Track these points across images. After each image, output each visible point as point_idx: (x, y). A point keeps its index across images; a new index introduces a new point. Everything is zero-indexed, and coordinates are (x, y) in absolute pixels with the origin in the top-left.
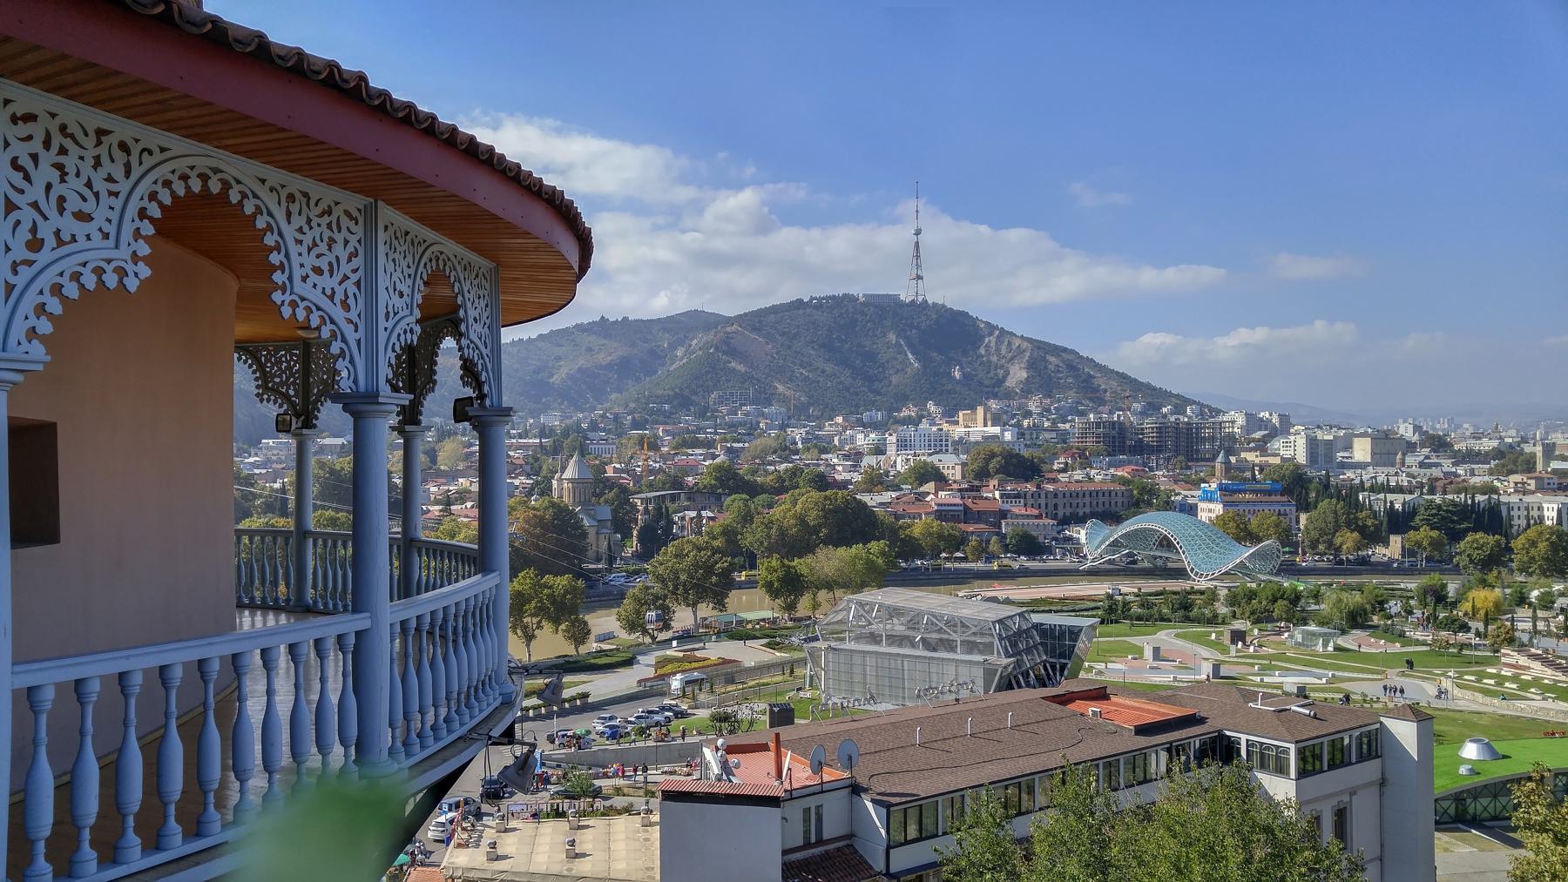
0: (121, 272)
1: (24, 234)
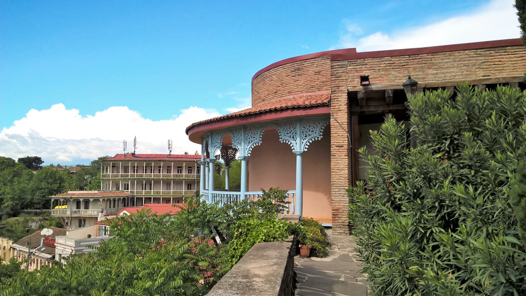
0: (318, 138)
1: (305, 135)
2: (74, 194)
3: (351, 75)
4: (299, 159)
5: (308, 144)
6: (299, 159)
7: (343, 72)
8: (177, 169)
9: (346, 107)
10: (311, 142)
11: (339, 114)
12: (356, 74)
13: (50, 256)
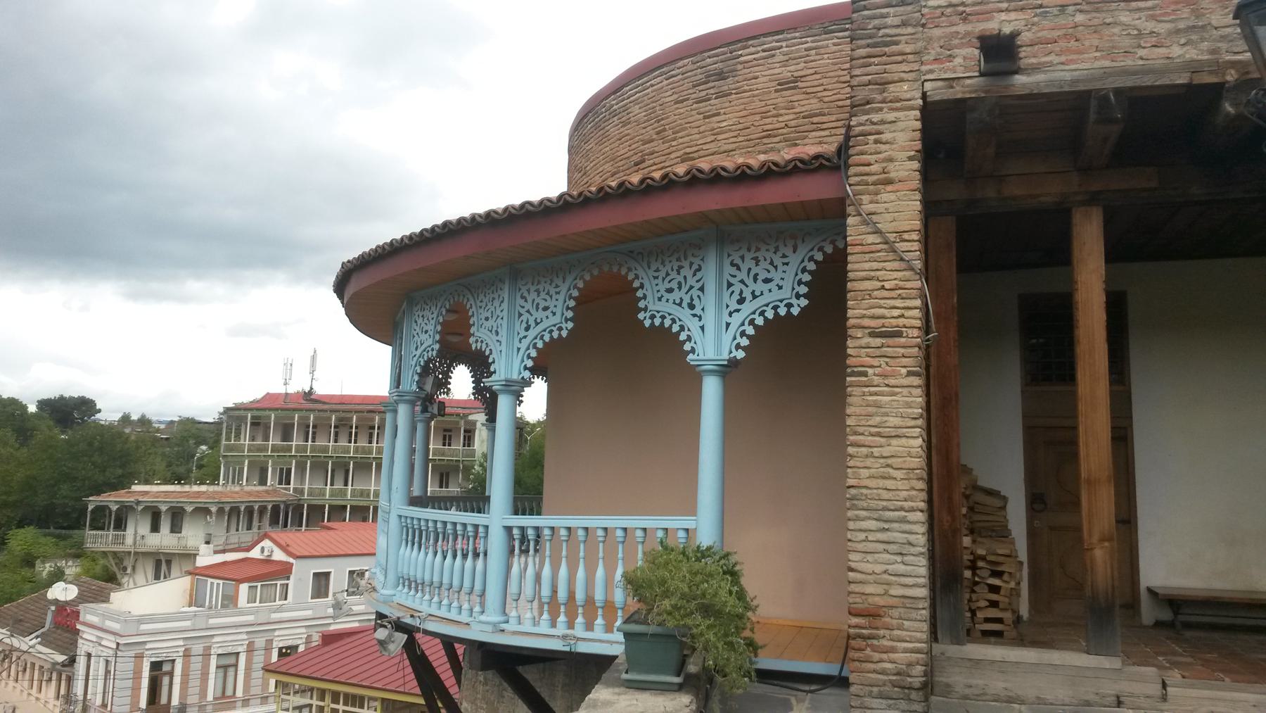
0: (789, 306)
1: (736, 297)
2: (146, 493)
3: (937, 32)
4: (711, 389)
5: (750, 331)
6: (711, 389)
7: (904, 24)
8: (442, 433)
9: (916, 165)
10: (760, 321)
11: (884, 197)
12: (962, 28)
13: (61, 658)
